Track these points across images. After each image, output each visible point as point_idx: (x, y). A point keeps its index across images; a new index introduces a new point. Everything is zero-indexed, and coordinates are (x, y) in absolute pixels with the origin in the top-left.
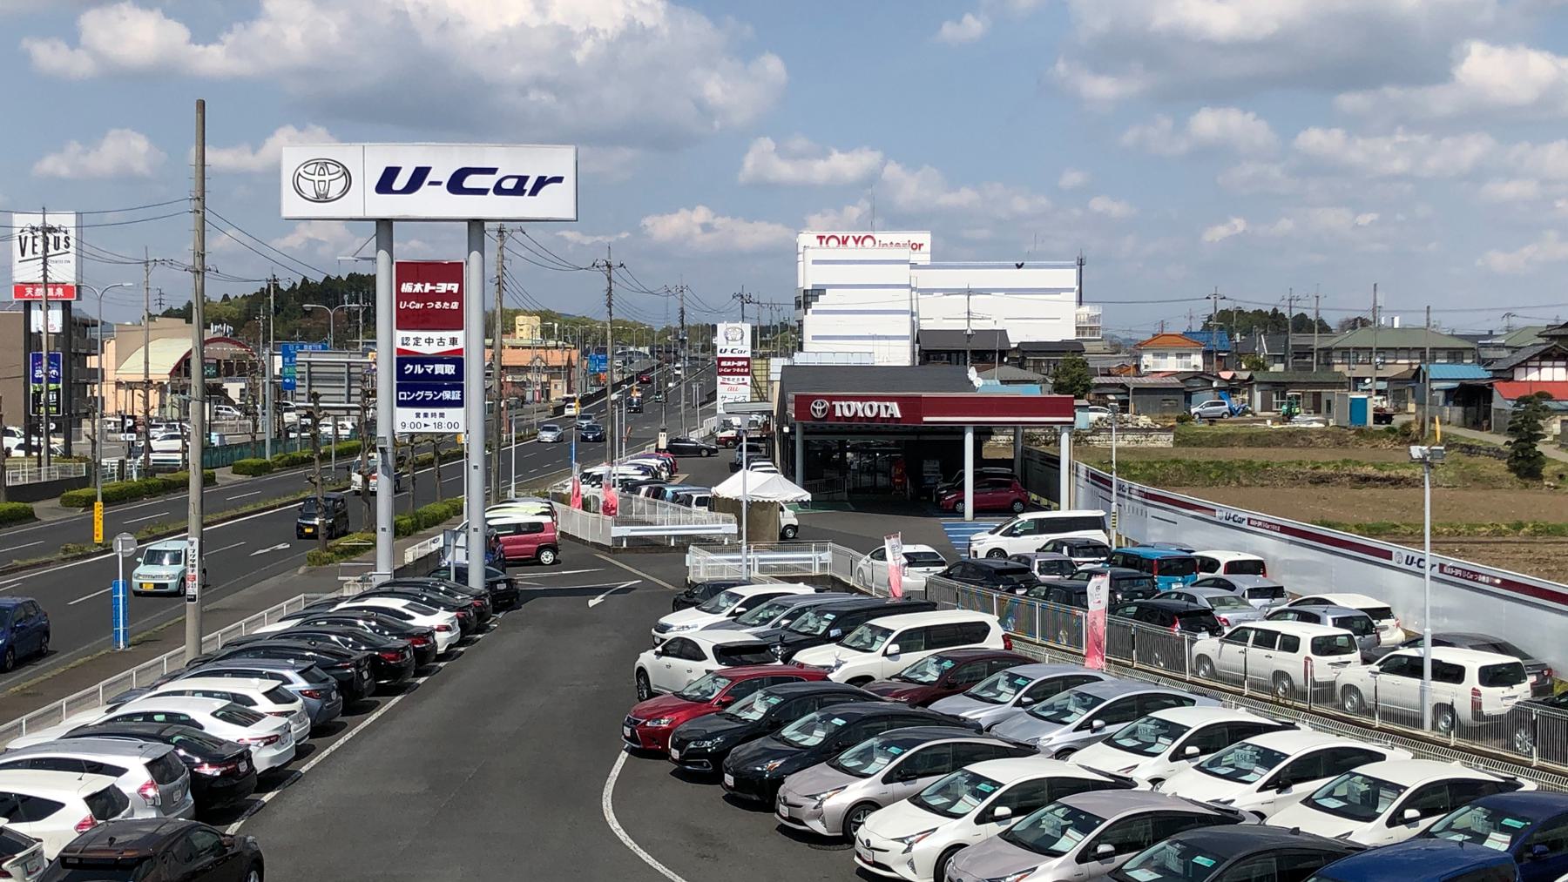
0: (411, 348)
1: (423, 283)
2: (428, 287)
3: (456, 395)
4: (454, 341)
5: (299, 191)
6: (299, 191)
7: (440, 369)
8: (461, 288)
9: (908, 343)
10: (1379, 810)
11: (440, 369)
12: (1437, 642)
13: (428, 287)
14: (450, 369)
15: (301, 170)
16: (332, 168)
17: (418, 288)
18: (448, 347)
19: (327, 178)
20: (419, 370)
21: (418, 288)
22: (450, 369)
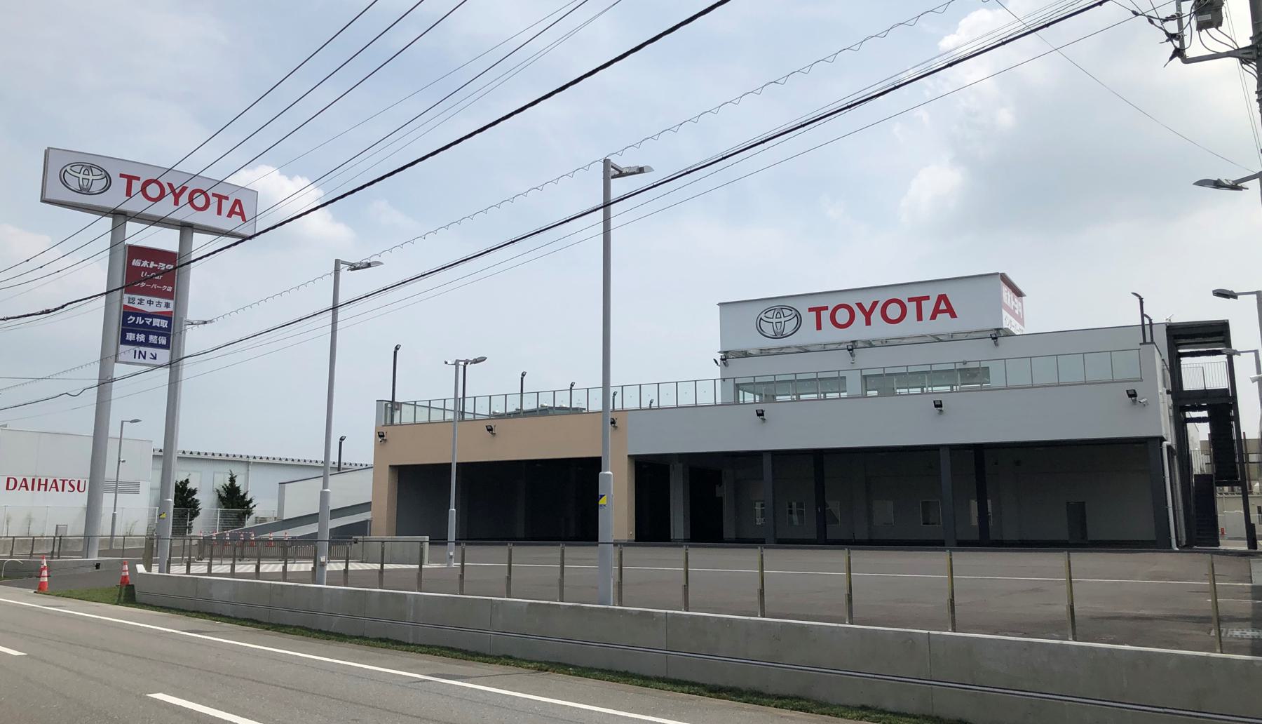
0: (136, 306)
1: (150, 261)
2: (152, 265)
3: (163, 341)
4: (167, 305)
5: (65, 183)
6: (65, 183)
7: (156, 322)
8: (130, 262)
9: (191, 314)
10: (718, 495)
11: (156, 322)
12: (839, 382)
13: (152, 265)
14: (164, 323)
15: (68, 168)
16: (96, 171)
17: (145, 264)
18: (163, 309)
19: (91, 177)
20: (140, 321)
21: (145, 264)
22: (164, 323)
